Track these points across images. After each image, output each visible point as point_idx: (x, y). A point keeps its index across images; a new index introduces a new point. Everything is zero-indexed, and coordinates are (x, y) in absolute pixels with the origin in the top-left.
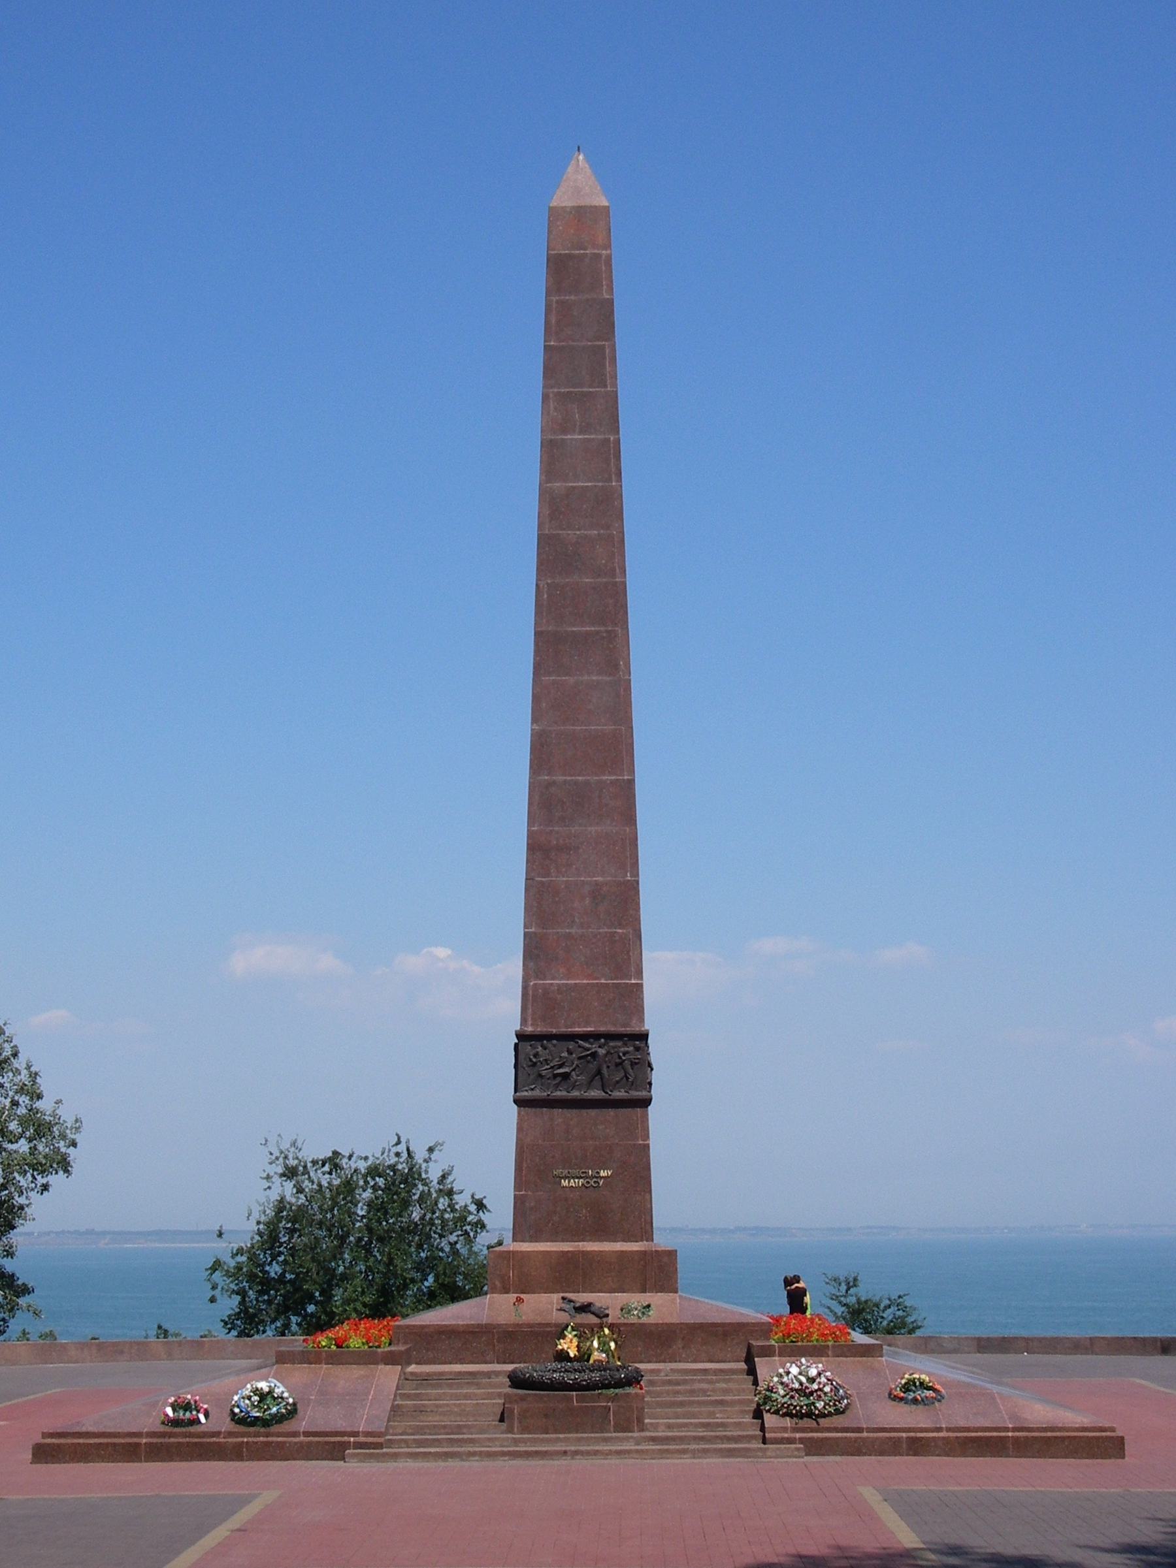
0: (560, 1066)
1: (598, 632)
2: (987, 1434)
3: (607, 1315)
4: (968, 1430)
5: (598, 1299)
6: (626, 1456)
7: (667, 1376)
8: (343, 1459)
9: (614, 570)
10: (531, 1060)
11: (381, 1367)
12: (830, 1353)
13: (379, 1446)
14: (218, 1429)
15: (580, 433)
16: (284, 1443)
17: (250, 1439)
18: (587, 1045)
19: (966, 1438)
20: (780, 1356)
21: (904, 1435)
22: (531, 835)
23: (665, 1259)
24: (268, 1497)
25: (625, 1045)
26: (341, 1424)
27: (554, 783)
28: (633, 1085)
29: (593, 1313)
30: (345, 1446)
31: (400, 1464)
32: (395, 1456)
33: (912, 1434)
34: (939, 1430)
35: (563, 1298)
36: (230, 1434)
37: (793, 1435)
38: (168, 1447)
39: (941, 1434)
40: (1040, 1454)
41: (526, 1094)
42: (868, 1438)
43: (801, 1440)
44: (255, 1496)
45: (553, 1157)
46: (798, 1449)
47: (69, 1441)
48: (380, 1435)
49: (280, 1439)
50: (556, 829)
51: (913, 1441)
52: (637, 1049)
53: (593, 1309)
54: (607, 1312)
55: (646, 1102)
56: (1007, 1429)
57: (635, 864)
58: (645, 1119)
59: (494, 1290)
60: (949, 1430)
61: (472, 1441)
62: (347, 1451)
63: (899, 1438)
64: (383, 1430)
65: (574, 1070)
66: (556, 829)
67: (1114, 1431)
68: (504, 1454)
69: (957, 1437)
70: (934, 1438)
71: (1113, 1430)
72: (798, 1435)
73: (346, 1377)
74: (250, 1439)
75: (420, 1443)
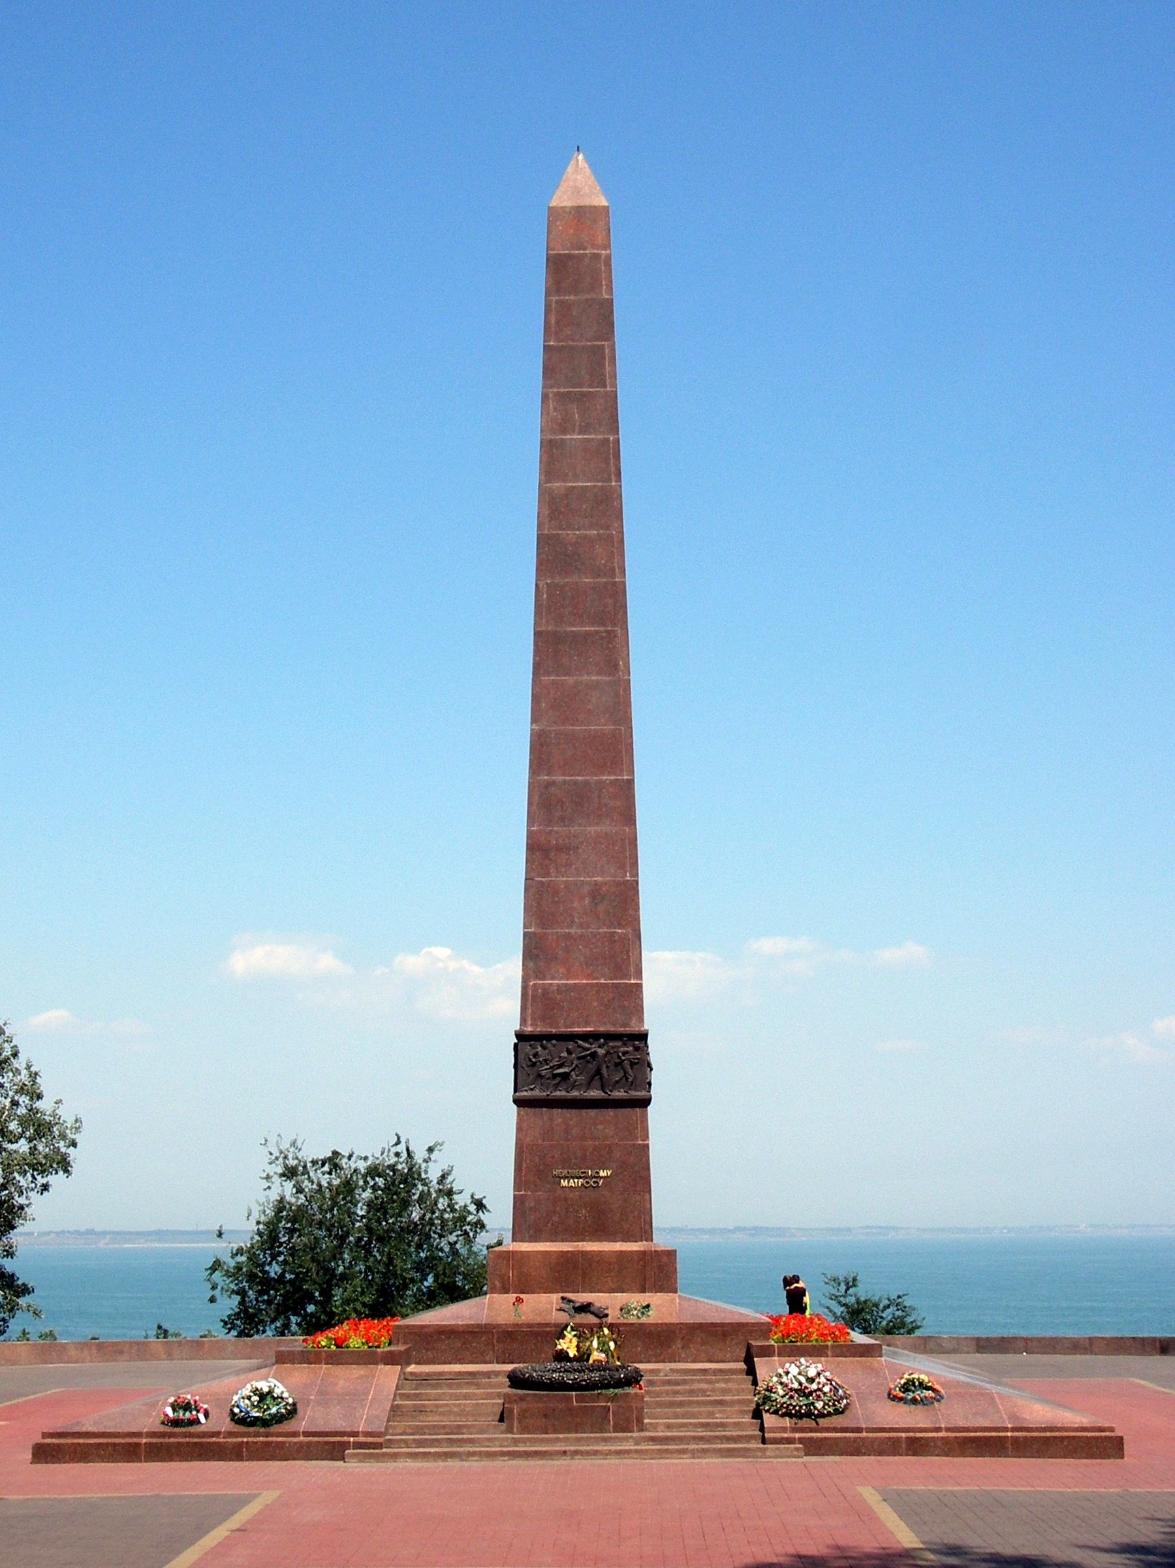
0: (560, 1066)
1: (597, 632)
2: (987, 1434)
3: (607, 1315)
4: (967, 1430)
5: (598, 1299)
6: (626, 1456)
7: (666, 1376)
8: (343, 1459)
9: (613, 570)
10: (530, 1060)
11: (381, 1367)
12: (829, 1353)
13: (379, 1446)
14: (217, 1429)
15: (579, 433)
16: (284, 1443)
17: (250, 1439)
18: (587, 1045)
19: (965, 1438)
20: (779, 1356)
21: (903, 1435)
22: (530, 835)
23: (665, 1259)
24: (268, 1497)
25: (625, 1045)
26: (340, 1424)
27: (554, 782)
28: (632, 1085)
29: (593, 1313)
30: (345, 1446)
31: (400, 1464)
32: (395, 1456)
33: (911, 1434)
34: (938, 1430)
35: (563, 1298)
36: (230, 1434)
37: (792, 1435)
38: (168, 1446)
39: (941, 1434)
40: (1039, 1454)
41: (525, 1094)
42: (868, 1438)
43: (801, 1440)
44: (255, 1496)
45: (553, 1157)
46: (797, 1449)
47: (69, 1441)
48: (379, 1435)
49: (280, 1439)
50: (555, 829)
51: (912, 1441)
52: (637, 1049)
53: (592, 1309)
54: (606, 1312)
55: (645, 1102)
56: (1006, 1429)
57: (635, 864)
58: (644, 1119)
59: (493, 1290)
60: (948, 1430)
61: (471, 1441)
62: (347, 1451)
63: (899, 1438)
64: (383, 1430)
65: (573, 1070)
66: (555, 829)
67: (1113, 1431)
68: (503, 1454)
69: (956, 1437)
70: (933, 1438)
71: (1112, 1430)
72: (797, 1435)
73: (346, 1377)
74: (250, 1439)
75: (420, 1443)
